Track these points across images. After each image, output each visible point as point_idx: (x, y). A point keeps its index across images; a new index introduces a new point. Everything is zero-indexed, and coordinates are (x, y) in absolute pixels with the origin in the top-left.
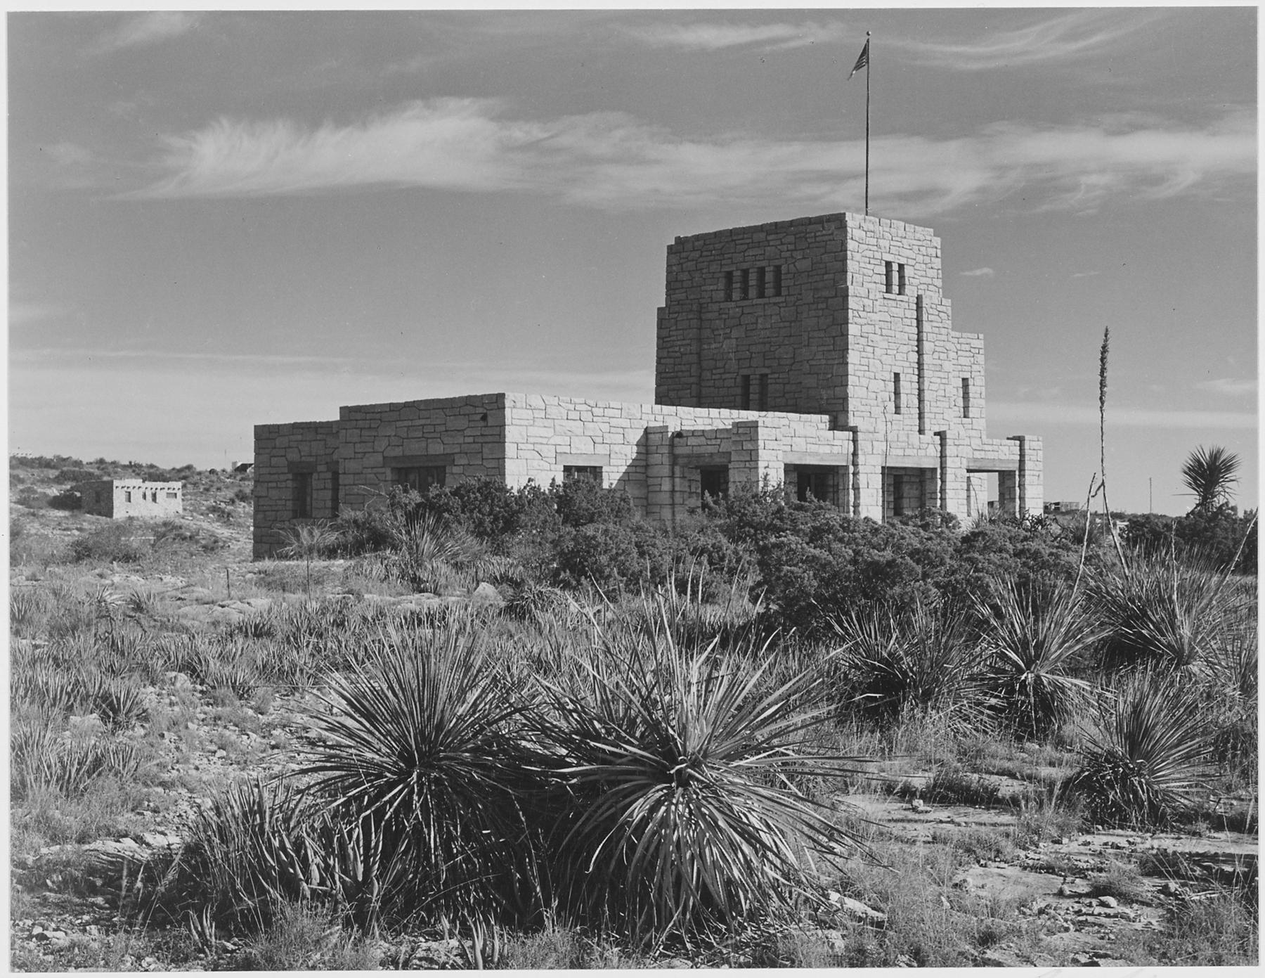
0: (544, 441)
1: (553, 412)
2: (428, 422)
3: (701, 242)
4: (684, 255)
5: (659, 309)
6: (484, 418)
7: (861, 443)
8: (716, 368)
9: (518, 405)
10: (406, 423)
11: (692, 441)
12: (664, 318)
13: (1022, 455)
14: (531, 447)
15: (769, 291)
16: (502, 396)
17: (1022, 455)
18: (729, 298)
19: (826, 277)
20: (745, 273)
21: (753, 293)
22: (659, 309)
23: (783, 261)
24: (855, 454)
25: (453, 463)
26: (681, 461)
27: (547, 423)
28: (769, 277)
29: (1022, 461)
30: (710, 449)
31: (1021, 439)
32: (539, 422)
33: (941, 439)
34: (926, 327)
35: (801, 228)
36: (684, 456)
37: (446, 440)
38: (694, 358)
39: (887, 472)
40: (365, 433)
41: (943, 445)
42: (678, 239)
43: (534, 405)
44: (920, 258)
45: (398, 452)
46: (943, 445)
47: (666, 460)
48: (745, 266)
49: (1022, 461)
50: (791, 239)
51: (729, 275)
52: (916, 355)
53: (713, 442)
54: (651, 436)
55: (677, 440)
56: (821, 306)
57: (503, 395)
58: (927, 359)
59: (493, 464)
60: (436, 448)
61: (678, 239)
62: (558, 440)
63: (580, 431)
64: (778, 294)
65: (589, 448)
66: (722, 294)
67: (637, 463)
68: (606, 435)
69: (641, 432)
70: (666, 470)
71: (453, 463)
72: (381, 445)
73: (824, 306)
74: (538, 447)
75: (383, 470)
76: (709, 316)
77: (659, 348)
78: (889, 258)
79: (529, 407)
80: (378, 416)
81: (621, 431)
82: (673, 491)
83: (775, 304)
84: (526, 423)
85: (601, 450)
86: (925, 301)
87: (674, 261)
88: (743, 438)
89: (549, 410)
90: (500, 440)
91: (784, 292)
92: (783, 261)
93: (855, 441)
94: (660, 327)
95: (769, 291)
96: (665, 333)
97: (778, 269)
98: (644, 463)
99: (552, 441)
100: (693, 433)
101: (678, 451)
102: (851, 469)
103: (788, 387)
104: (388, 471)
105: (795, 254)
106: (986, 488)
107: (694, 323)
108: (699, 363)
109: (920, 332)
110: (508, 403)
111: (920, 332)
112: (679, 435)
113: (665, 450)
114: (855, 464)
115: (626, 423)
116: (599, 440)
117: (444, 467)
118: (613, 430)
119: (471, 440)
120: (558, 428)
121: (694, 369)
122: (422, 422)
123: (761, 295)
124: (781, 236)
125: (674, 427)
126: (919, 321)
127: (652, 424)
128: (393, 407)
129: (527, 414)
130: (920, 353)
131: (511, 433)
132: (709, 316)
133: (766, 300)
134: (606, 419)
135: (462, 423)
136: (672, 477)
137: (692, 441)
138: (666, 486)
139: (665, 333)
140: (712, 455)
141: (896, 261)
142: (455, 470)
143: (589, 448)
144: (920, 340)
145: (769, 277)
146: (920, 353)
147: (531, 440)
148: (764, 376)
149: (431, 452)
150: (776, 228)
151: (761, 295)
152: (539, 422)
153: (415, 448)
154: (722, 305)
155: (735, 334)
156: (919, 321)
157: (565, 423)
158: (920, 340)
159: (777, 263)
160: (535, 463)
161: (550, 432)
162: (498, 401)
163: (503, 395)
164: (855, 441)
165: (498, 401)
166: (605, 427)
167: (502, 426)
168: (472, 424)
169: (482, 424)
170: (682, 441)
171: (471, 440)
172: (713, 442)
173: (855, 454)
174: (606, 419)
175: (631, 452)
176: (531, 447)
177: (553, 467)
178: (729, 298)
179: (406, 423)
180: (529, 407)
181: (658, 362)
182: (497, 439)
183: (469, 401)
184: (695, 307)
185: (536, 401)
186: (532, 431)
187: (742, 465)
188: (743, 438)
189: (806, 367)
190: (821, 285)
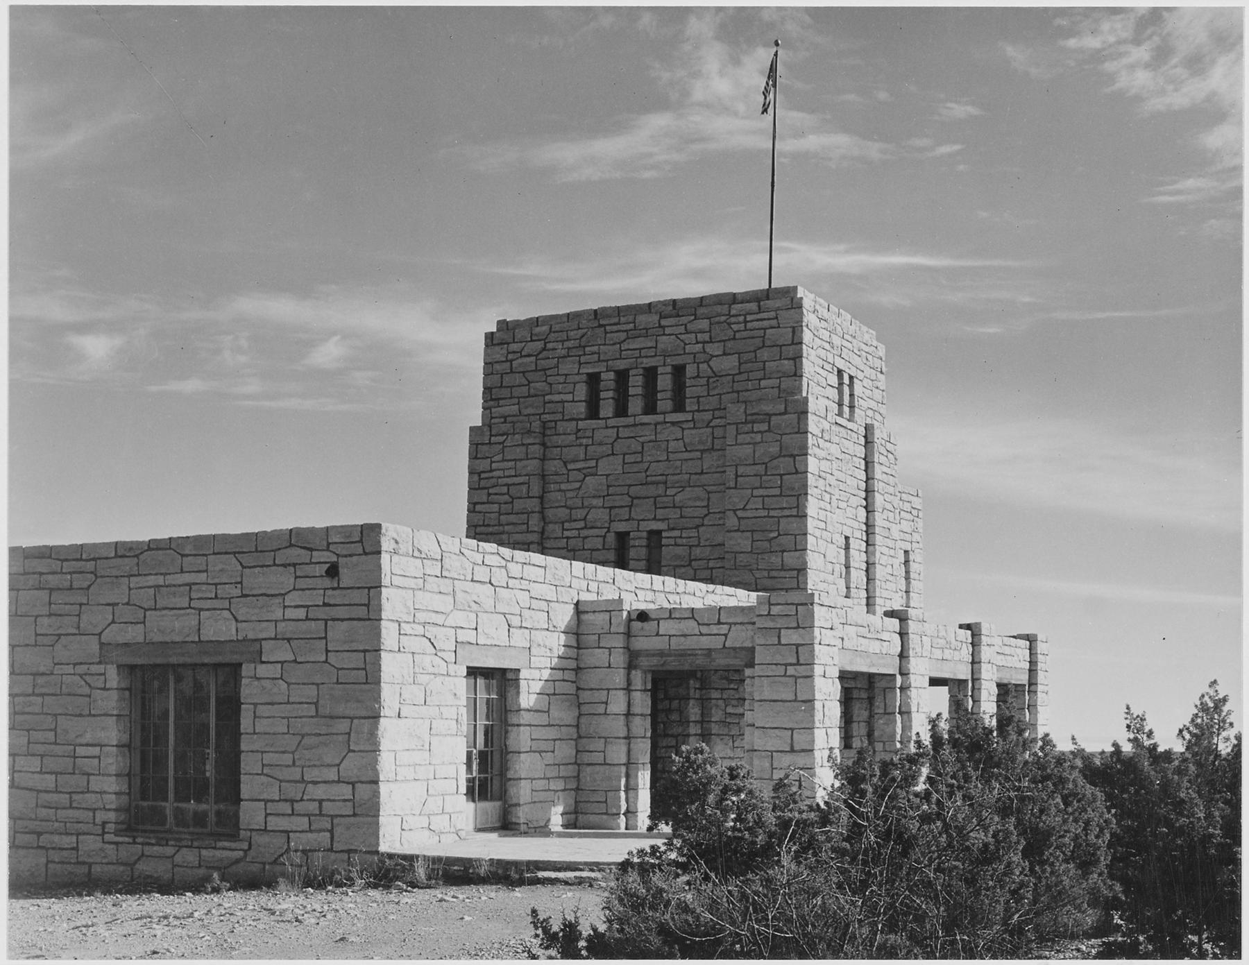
0: (439, 619)
1: (453, 563)
3: (545, 328)
4: (514, 347)
5: (472, 429)
6: (333, 571)
7: (913, 640)
8: (571, 520)
9: (403, 548)
10: (152, 580)
11: (666, 627)
12: (480, 443)
13: (1033, 662)
15: (664, 404)
17: (1033, 662)
18: (593, 413)
20: (622, 377)
21: (635, 405)
22: (472, 429)
23: (689, 359)
24: (903, 656)
25: (258, 658)
26: (644, 662)
27: (445, 585)
28: (664, 382)
29: (1032, 671)
30: (706, 642)
31: (1031, 639)
32: (432, 583)
33: (973, 635)
34: (878, 471)
35: (719, 309)
36: (649, 654)
37: (242, 613)
39: (844, 676)
40: (58, 597)
41: (975, 644)
43: (424, 549)
45: (134, 634)
46: (975, 644)
47: (619, 659)
48: (621, 365)
49: (1032, 671)
50: (704, 324)
51: (593, 380)
52: (863, 513)
53: (714, 629)
54: (584, 617)
55: (637, 625)
56: (757, 427)
57: (379, 526)
58: (879, 519)
59: (356, 660)
60: (219, 628)
62: (459, 618)
63: (488, 604)
64: (679, 407)
65: (502, 638)
66: (582, 408)
68: (526, 613)
69: (569, 611)
70: (619, 678)
71: (258, 658)
72: (96, 618)
73: (764, 427)
74: (431, 631)
75: (101, 668)
76: (559, 440)
77: (472, 489)
78: (840, 364)
79: (418, 554)
80: (90, 566)
81: (544, 605)
82: (628, 714)
83: (673, 423)
84: (411, 583)
85: (519, 638)
86: (879, 435)
87: (498, 357)
89: (446, 561)
90: (370, 615)
91: (690, 405)
92: (689, 359)
93: (903, 634)
94: (474, 456)
95: (664, 404)
96: (483, 465)
97: (679, 371)
98: (573, 664)
99: (450, 622)
100: (671, 614)
101: (640, 644)
102: (899, 679)
103: (697, 552)
104: (112, 671)
105: (710, 348)
106: (940, 701)
107: (536, 450)
108: (542, 512)
109: (869, 479)
110: (386, 545)
111: (869, 479)
112: (643, 616)
113: (619, 642)
114: (904, 673)
116: (515, 621)
118: (535, 604)
119: (301, 613)
120: (459, 595)
121: (535, 521)
122: (188, 578)
123: (650, 408)
124: (684, 320)
125: (632, 603)
126: (868, 464)
127: (585, 597)
128: (124, 551)
129: (414, 567)
130: (869, 509)
131: (393, 603)
132: (559, 440)
133: (660, 418)
134: (525, 584)
135: (281, 579)
137: (666, 627)
138: (618, 704)
139: (483, 465)
141: (849, 371)
142: (262, 670)
144: (869, 491)
145: (664, 382)
146: (869, 509)
147: (421, 617)
148: (655, 535)
149: (209, 634)
151: (650, 408)
152: (432, 583)
153: (173, 626)
155: (604, 466)
156: (868, 464)
157: (469, 586)
158: (869, 491)
159: (678, 361)
160: (427, 660)
161: (444, 603)
162: (366, 540)
164: (903, 634)
165: (366, 540)
166: (523, 598)
167: (375, 587)
168: (302, 583)
169: (327, 582)
170: (650, 626)
171: (301, 613)
172: (714, 629)
173: (903, 656)
174: (525, 584)
175: (556, 643)
178: (593, 413)
179: (152, 580)
180: (418, 554)
181: (471, 511)
182: (362, 612)
183: (295, 538)
184: (536, 425)
186: (424, 599)
187: (781, 670)
189: (732, 521)
190: (754, 395)
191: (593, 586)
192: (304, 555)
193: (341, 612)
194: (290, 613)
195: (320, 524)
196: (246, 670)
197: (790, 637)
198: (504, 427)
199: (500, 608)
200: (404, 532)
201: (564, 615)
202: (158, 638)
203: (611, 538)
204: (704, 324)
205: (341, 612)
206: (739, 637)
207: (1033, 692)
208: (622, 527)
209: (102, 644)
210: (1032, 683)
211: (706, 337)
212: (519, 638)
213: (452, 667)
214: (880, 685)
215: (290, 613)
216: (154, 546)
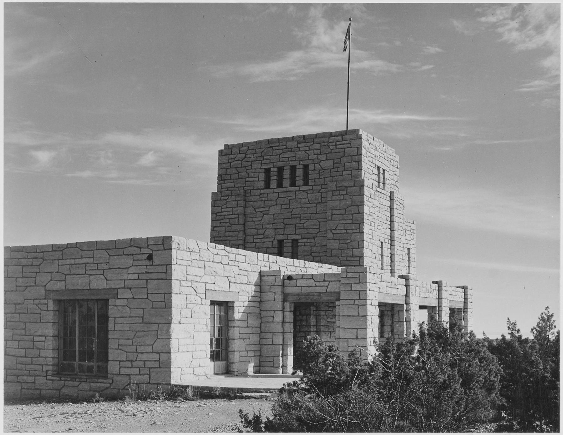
0: (198, 279)
1: (204, 254)
2: (91, 260)
3: (246, 148)
4: (232, 156)
5: (213, 193)
6: (150, 258)
7: (412, 288)
8: (257, 235)
10: (68, 262)
11: (300, 283)
12: (216, 200)
13: (466, 299)
14: (189, 284)
16: (170, 238)
17: (466, 299)
18: (267, 186)
19: (344, 173)
20: (280, 170)
21: (286, 183)
22: (213, 193)
23: (311, 162)
24: (407, 296)
25: (116, 296)
26: (290, 298)
27: (201, 264)
28: (300, 172)
29: (465, 302)
30: (318, 289)
31: (465, 288)
32: (195, 263)
33: (439, 286)
34: (396, 213)
35: (324, 139)
36: (293, 295)
38: (240, 227)
39: (380, 305)
41: (440, 290)
42: (227, 146)
43: (191, 247)
44: (391, 167)
45: (60, 286)
46: (440, 290)
47: (279, 297)
48: (280, 164)
49: (465, 302)
50: (318, 146)
51: (267, 171)
52: (389, 231)
53: (322, 284)
54: (263, 278)
55: (287, 282)
56: (341, 192)
57: (171, 237)
58: (396, 234)
59: (160, 298)
60: (99, 283)
61: (227, 146)
62: (207, 279)
63: (220, 272)
64: (306, 183)
65: (226, 287)
66: (262, 184)
67: (255, 299)
68: (237, 276)
69: (257, 275)
70: (279, 306)
71: (116, 296)
72: (43, 279)
73: (345, 192)
74: (194, 285)
75: (45, 301)
76: (252, 198)
78: (379, 164)
79: (189, 250)
80: (41, 255)
81: (245, 273)
82: (283, 322)
83: (303, 191)
84: (185, 263)
85: (234, 288)
86: (396, 196)
88: (352, 281)
90: (167, 277)
91: (311, 182)
92: (311, 162)
93: (407, 286)
94: (214, 206)
95: (299, 182)
96: (218, 209)
97: (306, 167)
98: (258, 299)
99: (203, 280)
100: (303, 277)
101: (288, 290)
103: (314, 249)
104: (50, 303)
106: (424, 316)
107: (242, 203)
109: (392, 216)
110: (174, 246)
111: (392, 216)
112: (290, 278)
113: (279, 289)
114: (407, 303)
115: (248, 267)
116: (232, 280)
117: (108, 300)
118: (241, 272)
119: (136, 276)
120: (207, 268)
121: (241, 235)
122: (85, 261)
123: (293, 184)
124: (308, 144)
125: (285, 272)
126: (391, 209)
127: (264, 269)
128: (56, 248)
129: (187, 256)
130: (392, 229)
131: (177, 272)
132: (252, 198)
133: (297, 188)
134: (236, 263)
135: (127, 261)
136: (283, 310)
137: (300, 283)
138: (279, 317)
139: (218, 209)
140: (320, 294)
141: (383, 167)
142: (118, 302)
143: (226, 287)
144: (392, 221)
145: (300, 172)
146: (392, 229)
147: (190, 278)
148: (295, 241)
149: (94, 286)
150: (304, 139)
152: (195, 263)
153: (78, 282)
154: (262, 191)
155: (272, 210)
156: (391, 209)
157: (212, 264)
158: (392, 221)
159: (306, 163)
160: (193, 297)
161: (201, 272)
162: (165, 243)
163: (171, 237)
164: (407, 286)
165: (165, 243)
166: (236, 269)
167: (169, 265)
168: (136, 263)
169: (147, 263)
170: (293, 282)
171: (136, 276)
172: (322, 284)
173: (407, 296)
174: (236, 263)
175: (251, 290)
176: (189, 284)
177: (204, 301)
178: (267, 186)
179: (68, 262)
180: (189, 250)
181: (212, 230)
182: (163, 276)
183: (133, 243)
184: (242, 192)
185: (192, 245)
186: (192, 270)
187: (352, 302)
188: (352, 281)
189: (330, 235)
190: (340, 178)
191: (267, 264)
192: (137, 250)
193: (154, 276)
194: (131, 276)
196: (111, 302)
197: (356, 287)
199: (226, 274)
200: (182, 240)
201: (254, 277)
202: (71, 288)
203: (275, 243)
204: (318, 146)
205: (154, 276)
206: (333, 287)
207: (466, 312)
208: (280, 237)
209: (46, 290)
210: (465, 308)
211: (318, 152)
212: (234, 288)
214: (397, 309)
215: (131, 276)
216: (69, 246)
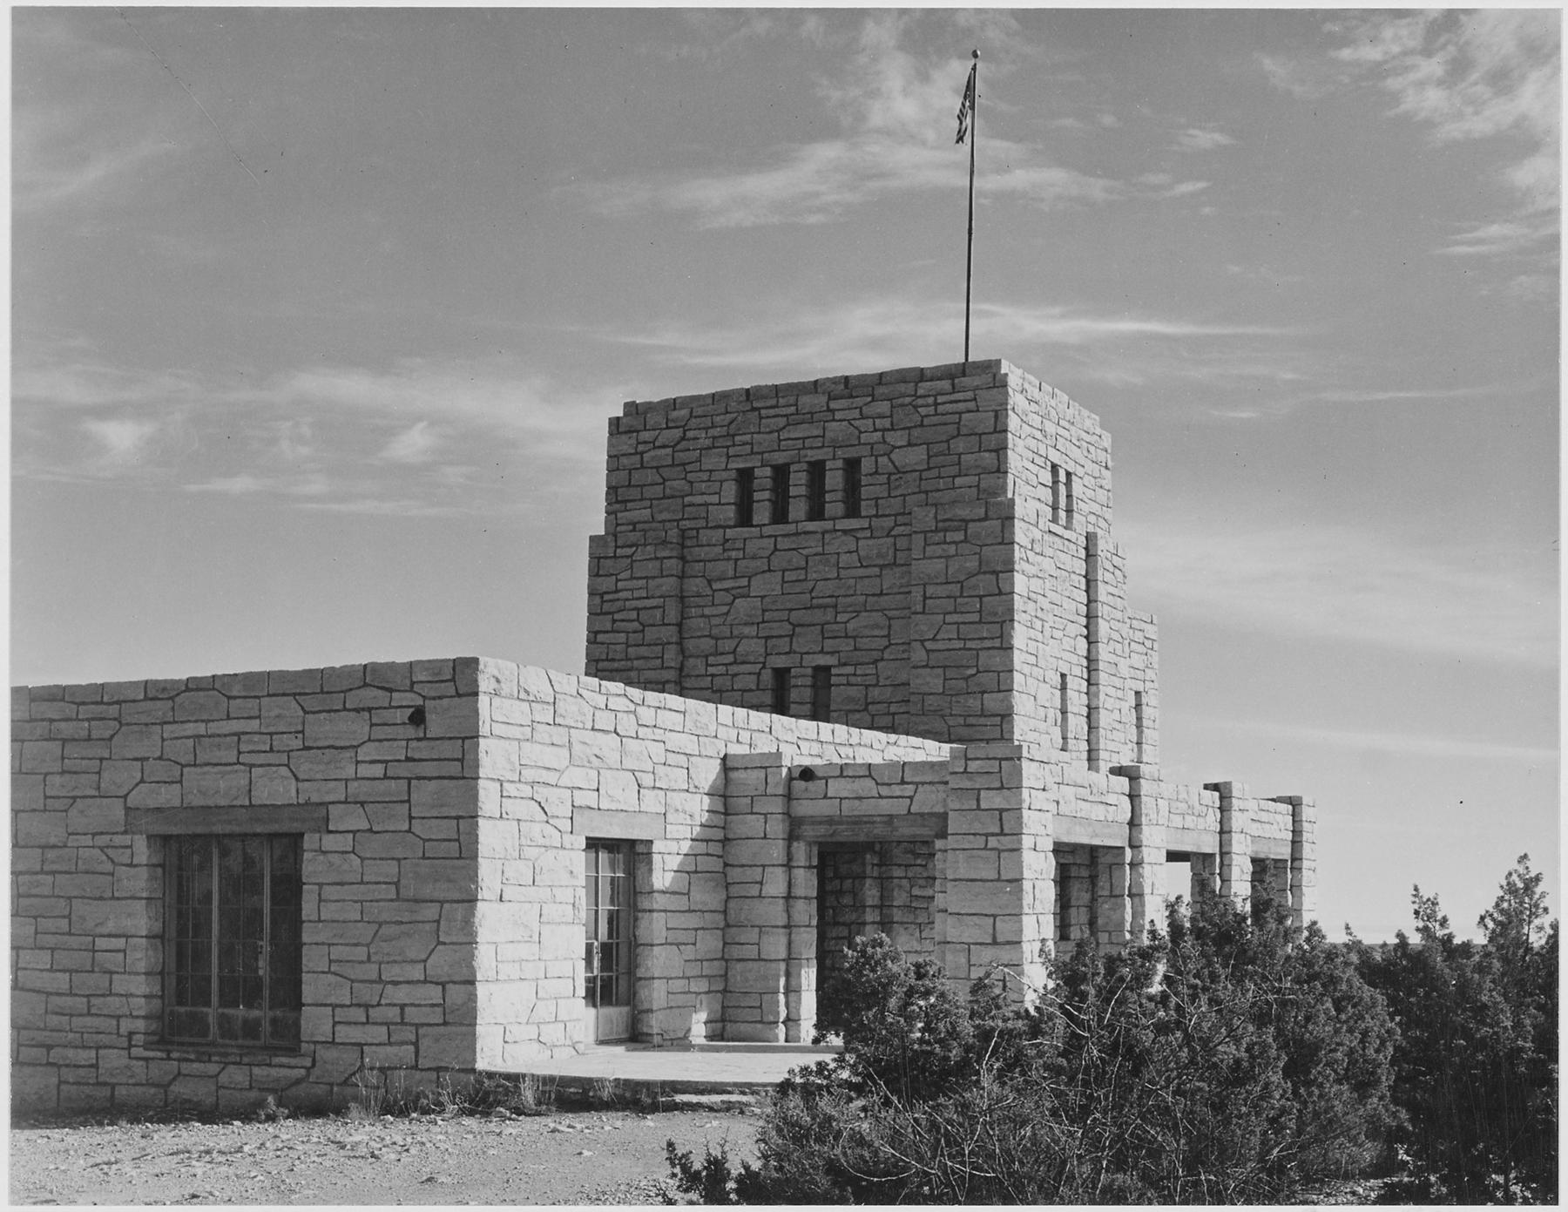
0: (551, 778)
1: (568, 707)
3: (684, 412)
4: (645, 436)
5: (592, 539)
6: (418, 718)
7: (1147, 803)
8: (717, 654)
9: (506, 688)
10: (190, 729)
11: (836, 787)
12: (603, 556)
13: (1297, 832)
15: (834, 507)
17: (1297, 832)
18: (745, 519)
20: (781, 474)
21: (798, 509)
22: (592, 539)
23: (865, 451)
24: (1134, 823)
25: (324, 827)
26: (809, 831)
27: (559, 735)
28: (834, 480)
29: (1296, 843)
30: (886, 807)
31: (1294, 803)
32: (543, 733)
33: (1221, 798)
34: (1102, 592)
35: (902, 388)
36: (815, 821)
37: (304, 770)
39: (1060, 849)
40: (72, 750)
41: (1224, 809)
43: (533, 689)
45: (168, 796)
46: (1224, 809)
47: (777, 827)
48: (780, 458)
49: (1296, 843)
50: (884, 407)
51: (745, 478)
52: (1083, 644)
53: (897, 790)
54: (733, 775)
55: (799, 785)
56: (950, 536)
57: (476, 661)
58: (1104, 652)
59: (447, 829)
60: (275, 789)
62: (576, 776)
63: (613, 758)
64: (853, 511)
65: (630, 801)
66: (730, 513)
68: (660, 770)
69: (715, 767)
70: (777, 852)
71: (324, 827)
72: (120, 776)
73: (960, 536)
74: (542, 793)
75: (126, 839)
76: (702, 553)
77: (593, 614)
78: (1055, 457)
79: (525, 696)
80: (113, 710)
81: (682, 760)
82: (789, 897)
83: (845, 532)
84: (516, 732)
85: (652, 802)
86: (1103, 546)
87: (625, 449)
89: (559, 704)
90: (464, 772)
91: (866, 508)
92: (865, 451)
93: (1133, 797)
94: (595, 573)
95: (834, 507)
96: (607, 584)
97: (852, 466)
98: (720, 834)
99: (565, 781)
100: (843, 771)
101: (803, 808)
102: (1128, 853)
103: (875, 693)
104: (141, 843)
105: (891, 438)
106: (1180, 880)
107: (673, 565)
108: (680, 643)
109: (1091, 601)
110: (485, 684)
111: (1091, 601)
112: (807, 774)
113: (777, 806)
114: (1135, 846)
116: (647, 780)
118: (672, 758)
119: (378, 770)
120: (577, 747)
121: (671, 655)
122: (236, 726)
123: (816, 513)
124: (859, 401)
125: (794, 758)
126: (1090, 582)
127: (735, 749)
128: (155, 692)
129: (519, 712)
130: (1091, 639)
131: (493, 758)
132: (702, 553)
133: (828, 525)
134: (659, 734)
135: (353, 728)
137: (836, 787)
138: (776, 884)
139: (607, 584)
141: (1066, 465)
142: (329, 842)
144: (1091, 617)
145: (834, 480)
146: (1091, 639)
147: (529, 775)
148: (822, 672)
149: (262, 796)
151: (816, 513)
152: (543, 733)
153: (218, 787)
155: (758, 586)
156: (1090, 582)
157: (589, 736)
158: (1091, 617)
159: (852, 453)
160: (536, 829)
161: (558, 758)
162: (459, 678)
164: (1133, 797)
165: (459, 678)
166: (657, 751)
167: (470, 737)
168: (379, 733)
169: (411, 731)
170: (815, 787)
171: (378, 770)
172: (897, 790)
173: (1134, 823)
174: (659, 734)
175: (698, 808)
178: (745, 519)
179: (190, 729)
180: (525, 696)
181: (592, 641)
182: (454, 768)
183: (371, 676)
184: (673, 534)
186: (533, 753)
187: (980, 842)
189: (919, 655)
190: (947, 496)
191: (745, 736)
192: (381, 698)
193: (428, 769)
194: (364, 770)
195: (402, 658)
196: (309, 841)
197: (991, 800)
198: (633, 537)
199: (628, 764)
200: (507, 668)
201: (709, 773)
202: (198, 801)
203: (767, 676)
204: (884, 407)
205: (428, 769)
206: (928, 800)
207: (1297, 870)
208: (781, 662)
209: (128, 809)
210: (1296, 857)
211: (887, 423)
212: (652, 802)
213: (567, 838)
214: (1104, 860)
215: (364, 770)
216: (193, 686)
